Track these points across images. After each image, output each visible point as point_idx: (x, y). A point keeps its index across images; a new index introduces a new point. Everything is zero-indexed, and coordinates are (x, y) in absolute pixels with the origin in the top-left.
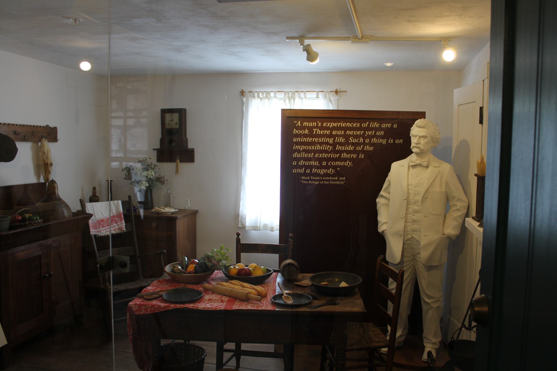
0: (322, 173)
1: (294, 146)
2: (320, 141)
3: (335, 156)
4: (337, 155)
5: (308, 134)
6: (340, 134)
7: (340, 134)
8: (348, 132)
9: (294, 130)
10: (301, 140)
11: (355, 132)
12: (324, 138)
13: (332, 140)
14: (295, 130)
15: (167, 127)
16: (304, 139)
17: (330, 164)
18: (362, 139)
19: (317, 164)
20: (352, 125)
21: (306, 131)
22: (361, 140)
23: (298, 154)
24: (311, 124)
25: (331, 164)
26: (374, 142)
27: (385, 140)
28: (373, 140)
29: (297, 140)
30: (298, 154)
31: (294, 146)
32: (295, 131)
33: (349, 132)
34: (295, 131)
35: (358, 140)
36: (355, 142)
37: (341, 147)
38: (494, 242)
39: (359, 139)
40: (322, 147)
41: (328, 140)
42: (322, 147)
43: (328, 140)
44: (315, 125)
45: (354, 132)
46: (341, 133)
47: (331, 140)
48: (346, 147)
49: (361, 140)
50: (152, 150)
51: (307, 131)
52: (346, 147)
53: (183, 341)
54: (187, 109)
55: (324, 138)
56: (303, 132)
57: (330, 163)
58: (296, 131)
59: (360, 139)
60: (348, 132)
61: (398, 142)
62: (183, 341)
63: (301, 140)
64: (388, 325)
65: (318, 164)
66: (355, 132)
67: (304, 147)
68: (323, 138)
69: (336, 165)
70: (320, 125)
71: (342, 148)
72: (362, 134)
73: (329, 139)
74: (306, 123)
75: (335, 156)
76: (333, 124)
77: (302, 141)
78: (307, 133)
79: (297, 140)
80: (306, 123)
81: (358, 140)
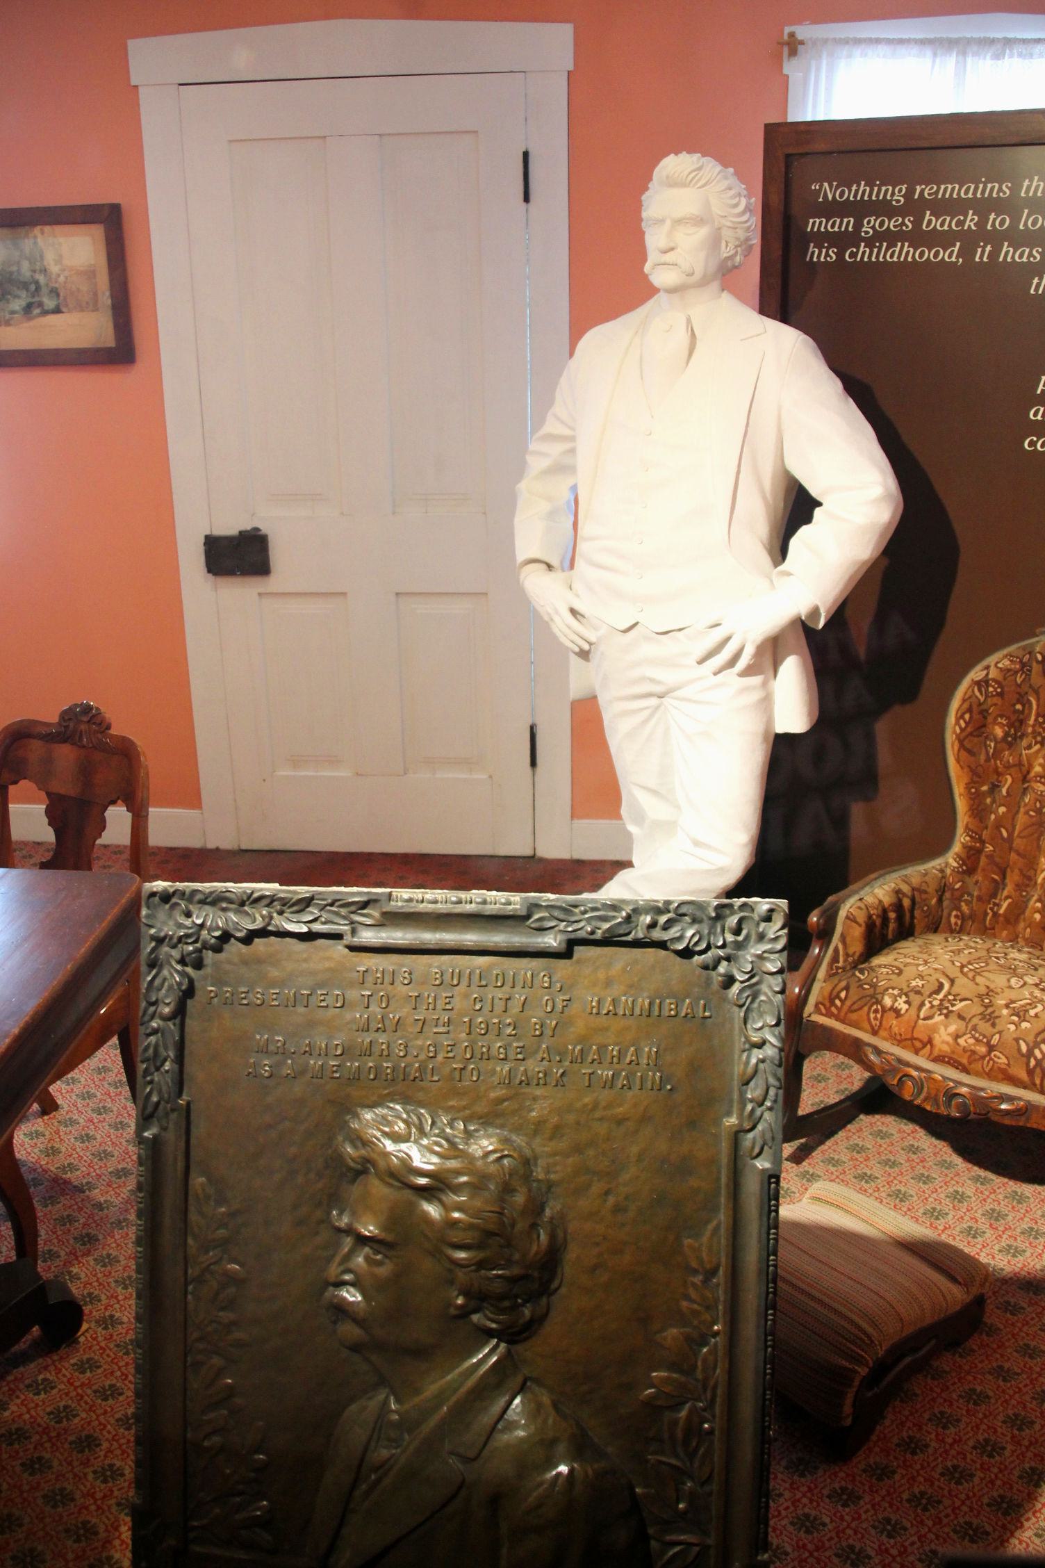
1: (980, 250)
3: (842, 195)
6: (1025, 259)
7: (1025, 259)
14: (927, 218)
15: (233, 940)
16: (884, 188)
17: (1030, 445)
18: (1042, 184)
21: (969, 217)
24: (835, 222)
25: (1035, 446)
27: (900, 191)
31: (980, 250)
32: (930, 222)
34: (930, 222)
39: (962, 218)
40: (876, 250)
42: (876, 250)
44: (850, 229)
46: (1028, 258)
51: (971, 220)
54: (122, 206)
57: (1032, 444)
58: (933, 219)
59: (858, 251)
61: (970, 195)
63: (870, 195)
73: (890, 188)
74: (818, 221)
75: (842, 195)
80: (818, 221)
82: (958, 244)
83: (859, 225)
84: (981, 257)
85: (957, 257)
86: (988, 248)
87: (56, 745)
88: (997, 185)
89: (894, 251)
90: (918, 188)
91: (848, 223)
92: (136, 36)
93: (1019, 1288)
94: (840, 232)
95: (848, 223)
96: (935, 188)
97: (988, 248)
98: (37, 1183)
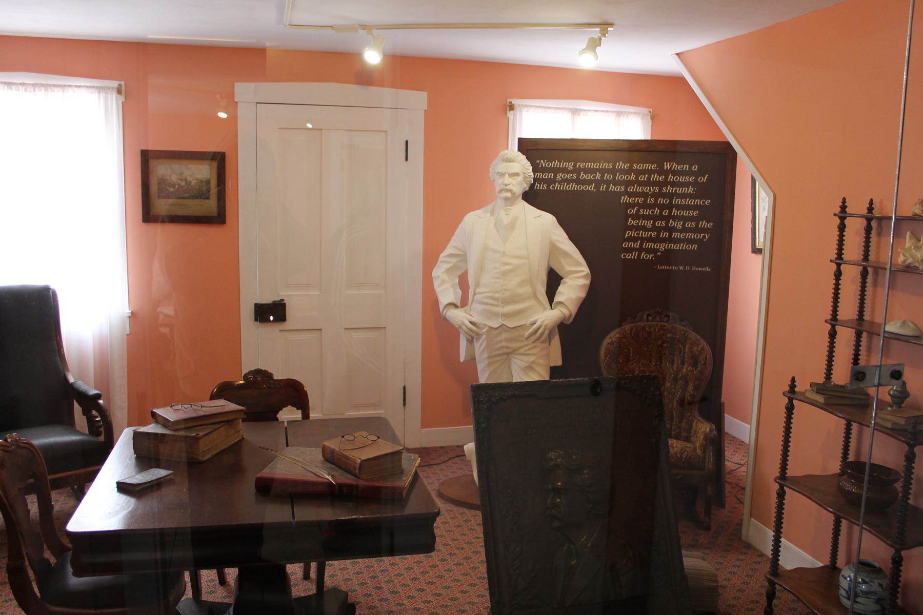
5: (693, 193)
8: (660, 201)
9: (581, 173)
10: (540, 187)
12: (684, 244)
13: (573, 164)
18: (659, 211)
19: (592, 189)
20: (703, 202)
22: (657, 212)
23: (638, 188)
26: (703, 226)
28: (702, 224)
29: (682, 191)
30: (638, 188)
32: (583, 176)
33: (662, 199)
34: (583, 176)
36: (647, 213)
37: (607, 164)
38: (4, 525)
41: (645, 223)
43: (645, 223)
47: (571, 164)
49: (657, 212)
55: (684, 244)
56: (627, 177)
59: (655, 210)
60: (660, 201)
63: (540, 187)
65: (594, 189)
67: (589, 189)
68: (682, 244)
71: (608, 166)
73: (646, 222)
76: (591, 188)
77: (561, 189)
78: (692, 192)
79: (682, 191)
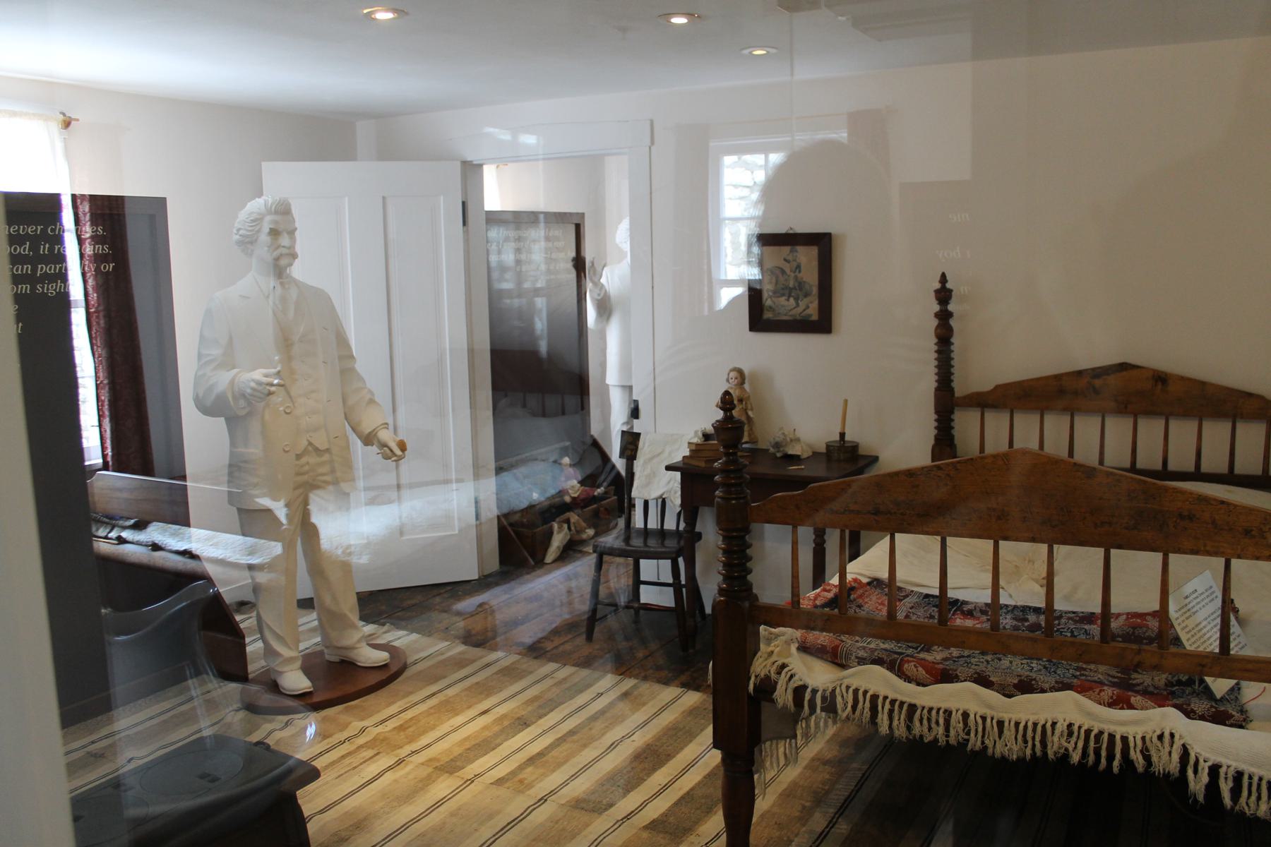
0: (52, 293)
1: (42, 247)
2: (39, 290)
4: (109, 266)
11: (22, 227)
24: (18, 268)
31: (42, 247)
35: (52, 228)
45: (19, 228)
48: (46, 285)
50: (943, 271)
52: (46, 285)
53: (683, 582)
59: (56, 228)
62: (683, 582)
64: (1206, 678)
66: (22, 227)
67: (48, 271)
69: (19, 292)
70: (40, 289)
72: (38, 233)
81: (52, 228)
82: (28, 243)
83: (34, 270)
84: (44, 251)
85: (29, 251)
86: (47, 246)
87: (897, 579)
88: (101, 246)
89: (41, 271)
90: (57, 247)
91: (27, 268)
92: (674, 591)
93: (1191, 518)
94: (22, 275)
95: (27, 268)
96: (35, 228)
97: (47, 246)
98: (659, 668)
